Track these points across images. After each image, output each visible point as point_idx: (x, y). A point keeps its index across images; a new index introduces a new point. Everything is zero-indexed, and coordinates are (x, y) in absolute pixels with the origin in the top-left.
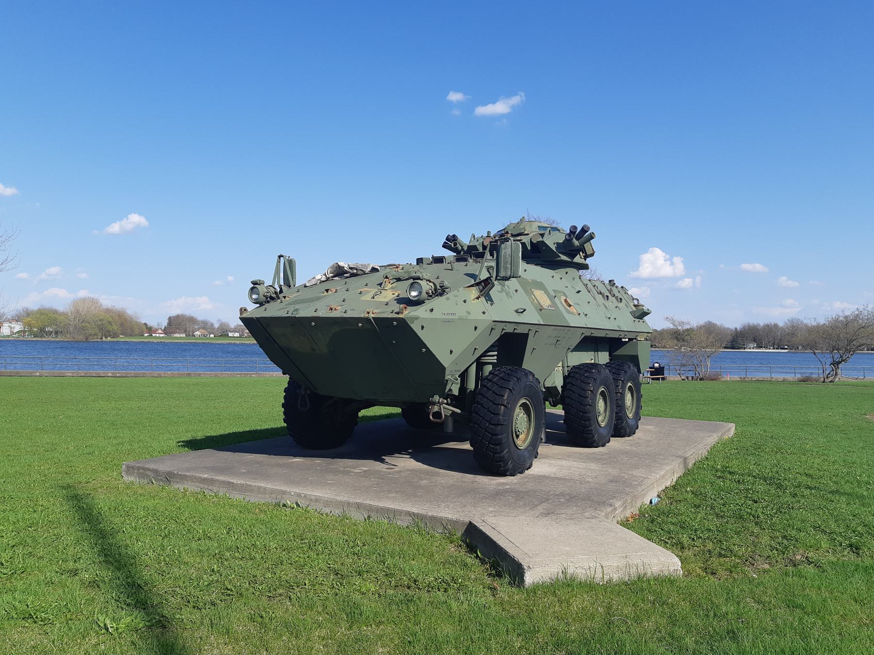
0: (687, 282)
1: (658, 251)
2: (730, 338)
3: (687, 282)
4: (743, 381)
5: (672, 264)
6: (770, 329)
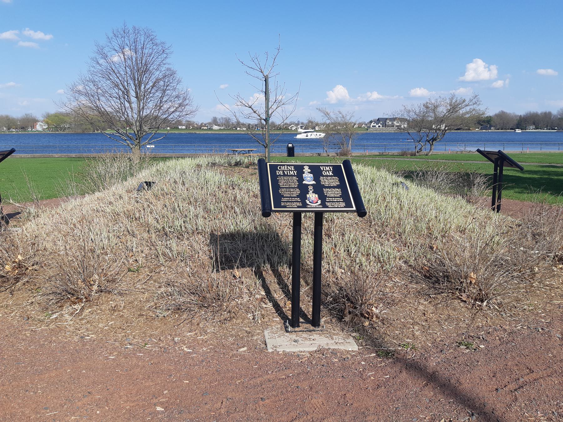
0: (499, 84)
1: (480, 62)
2: (516, 122)
3: (499, 84)
4: (381, 155)
5: (489, 70)
6: (547, 115)
